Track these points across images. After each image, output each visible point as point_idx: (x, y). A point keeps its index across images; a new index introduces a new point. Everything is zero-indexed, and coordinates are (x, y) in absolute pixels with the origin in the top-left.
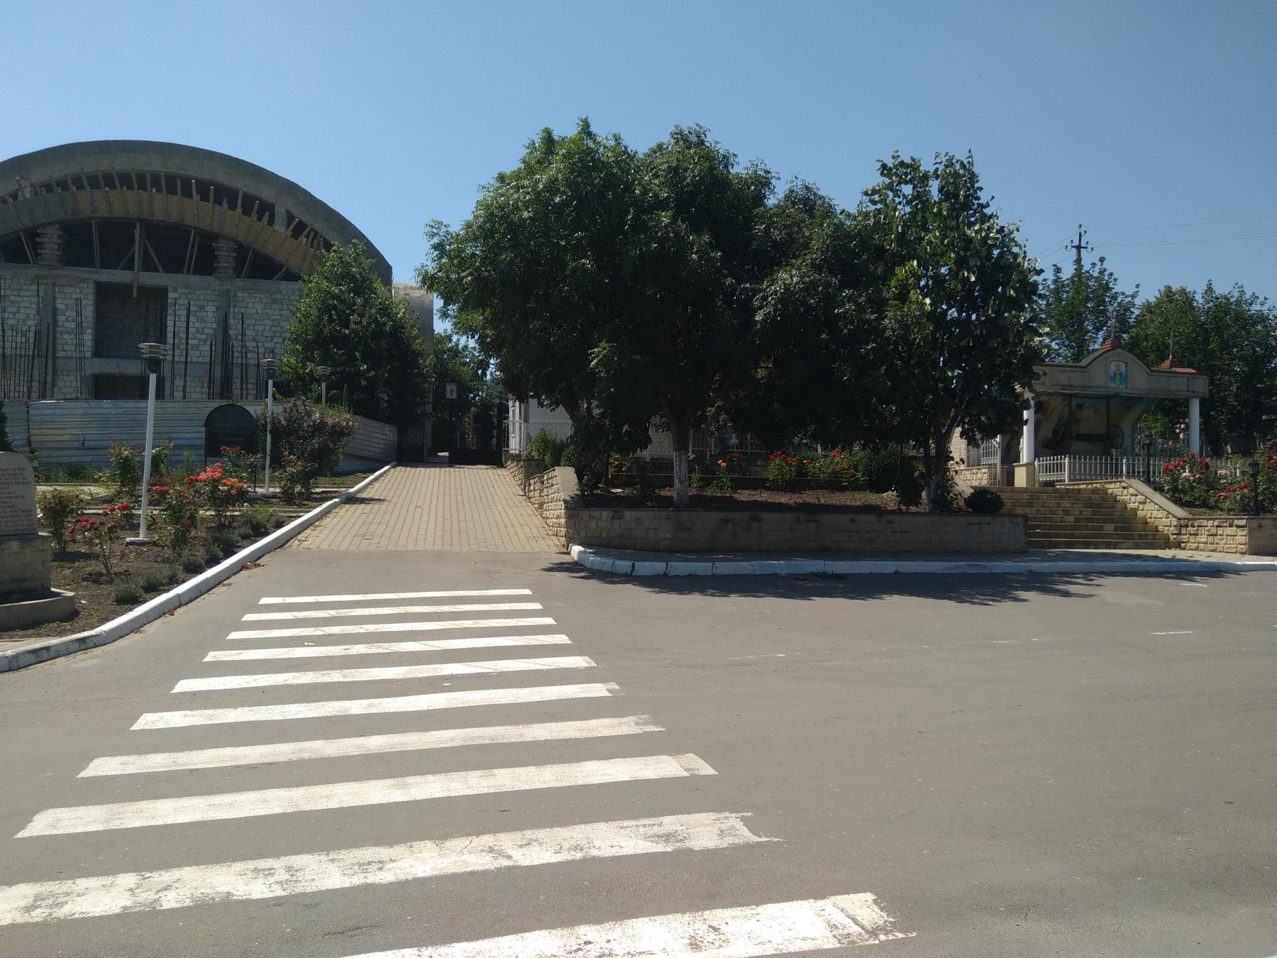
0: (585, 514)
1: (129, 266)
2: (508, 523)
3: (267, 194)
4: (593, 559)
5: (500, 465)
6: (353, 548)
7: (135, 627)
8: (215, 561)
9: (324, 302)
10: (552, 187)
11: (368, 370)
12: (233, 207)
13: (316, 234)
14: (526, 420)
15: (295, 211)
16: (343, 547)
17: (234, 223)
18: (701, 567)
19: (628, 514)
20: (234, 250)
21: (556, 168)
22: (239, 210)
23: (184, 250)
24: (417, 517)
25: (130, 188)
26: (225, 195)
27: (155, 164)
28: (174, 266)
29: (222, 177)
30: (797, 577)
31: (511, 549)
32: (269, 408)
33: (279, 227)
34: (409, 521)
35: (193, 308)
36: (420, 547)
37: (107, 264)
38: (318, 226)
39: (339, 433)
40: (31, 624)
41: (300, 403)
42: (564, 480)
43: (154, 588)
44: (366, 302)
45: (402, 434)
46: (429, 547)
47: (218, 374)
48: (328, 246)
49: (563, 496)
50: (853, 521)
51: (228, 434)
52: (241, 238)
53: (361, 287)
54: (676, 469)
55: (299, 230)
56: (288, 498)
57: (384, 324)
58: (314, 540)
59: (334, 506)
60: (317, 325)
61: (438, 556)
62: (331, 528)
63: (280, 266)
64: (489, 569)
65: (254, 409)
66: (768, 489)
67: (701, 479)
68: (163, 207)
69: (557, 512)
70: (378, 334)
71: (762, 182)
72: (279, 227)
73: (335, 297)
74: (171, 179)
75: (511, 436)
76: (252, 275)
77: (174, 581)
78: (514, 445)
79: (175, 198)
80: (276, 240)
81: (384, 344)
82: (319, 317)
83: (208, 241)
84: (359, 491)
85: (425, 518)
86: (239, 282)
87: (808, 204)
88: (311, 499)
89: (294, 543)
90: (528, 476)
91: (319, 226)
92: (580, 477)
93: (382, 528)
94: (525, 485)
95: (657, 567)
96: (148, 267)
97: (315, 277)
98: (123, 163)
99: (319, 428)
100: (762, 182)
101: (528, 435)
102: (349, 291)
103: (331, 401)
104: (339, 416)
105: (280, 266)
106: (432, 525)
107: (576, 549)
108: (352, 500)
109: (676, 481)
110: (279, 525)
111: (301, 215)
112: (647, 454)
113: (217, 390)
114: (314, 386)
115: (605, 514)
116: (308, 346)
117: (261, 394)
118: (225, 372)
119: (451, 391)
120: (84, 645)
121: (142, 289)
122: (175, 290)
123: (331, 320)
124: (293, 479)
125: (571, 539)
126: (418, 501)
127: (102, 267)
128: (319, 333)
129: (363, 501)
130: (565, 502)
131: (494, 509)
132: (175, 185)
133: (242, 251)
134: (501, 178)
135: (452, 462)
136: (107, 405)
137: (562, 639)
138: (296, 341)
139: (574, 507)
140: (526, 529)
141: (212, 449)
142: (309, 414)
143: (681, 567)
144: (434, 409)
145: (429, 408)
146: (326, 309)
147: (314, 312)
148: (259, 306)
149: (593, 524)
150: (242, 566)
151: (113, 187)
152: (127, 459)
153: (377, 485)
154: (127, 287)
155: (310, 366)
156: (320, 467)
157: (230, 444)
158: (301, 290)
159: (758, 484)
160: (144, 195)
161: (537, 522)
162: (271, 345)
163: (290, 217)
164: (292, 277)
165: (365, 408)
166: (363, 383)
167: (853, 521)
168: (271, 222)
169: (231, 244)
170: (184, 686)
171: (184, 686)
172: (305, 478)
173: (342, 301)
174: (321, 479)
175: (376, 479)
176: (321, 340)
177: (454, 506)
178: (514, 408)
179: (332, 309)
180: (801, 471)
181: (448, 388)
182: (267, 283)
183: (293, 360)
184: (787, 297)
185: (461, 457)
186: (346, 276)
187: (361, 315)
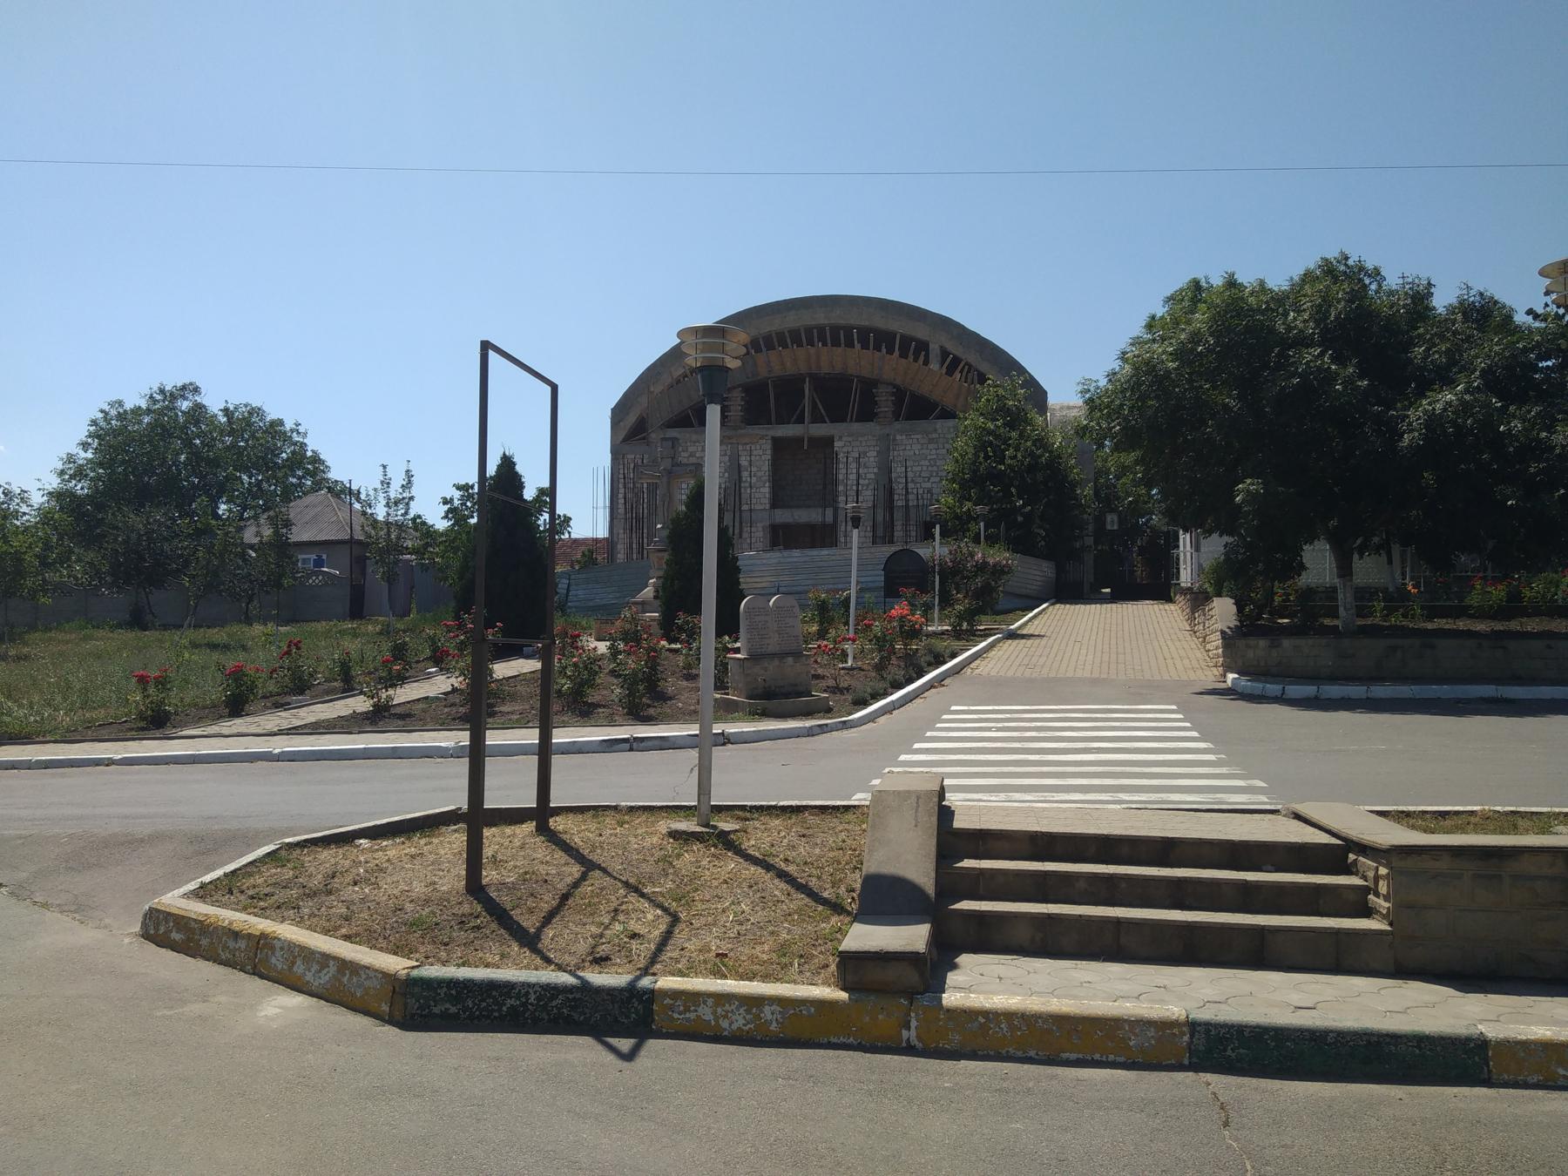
0: (1241, 643)
1: (801, 420)
2: (1167, 655)
3: (920, 332)
4: (1245, 683)
5: (1170, 600)
6: (1019, 674)
7: (871, 718)
8: (911, 681)
9: (979, 438)
10: (1195, 338)
11: (1024, 506)
12: (890, 351)
13: (970, 366)
14: (1197, 549)
15: (949, 346)
16: (1010, 674)
17: (891, 367)
18: (1356, 691)
19: (1287, 643)
20: (893, 394)
21: (1200, 319)
22: (897, 353)
23: (845, 399)
24: (1077, 649)
25: (800, 345)
26: (883, 340)
27: (820, 318)
28: (838, 417)
29: (880, 322)
30: (1459, 701)
31: (1166, 677)
32: (937, 550)
33: (934, 366)
34: (1067, 655)
35: (857, 452)
36: (1079, 674)
37: (781, 421)
38: (971, 362)
39: (1000, 571)
40: (808, 713)
41: (965, 545)
42: (1223, 611)
43: (876, 697)
44: (1021, 436)
45: (1060, 570)
46: (1087, 674)
47: (880, 518)
48: (982, 379)
49: (1219, 626)
50: (1549, 647)
51: (904, 576)
52: (898, 381)
53: (1016, 419)
54: (1340, 596)
55: (953, 364)
56: (957, 634)
57: (1040, 456)
58: (983, 668)
59: (998, 641)
60: (974, 463)
61: (1095, 682)
62: (997, 658)
63: (934, 405)
64: (1141, 691)
65: (924, 551)
66: (1471, 617)
67: (1385, 608)
68: (831, 360)
69: (1216, 641)
70: (1033, 468)
71: (1420, 298)
72: (934, 366)
73: (990, 433)
74: (835, 329)
75: (1182, 567)
76: (911, 417)
77: (885, 694)
78: (1186, 577)
79: (840, 350)
80: (931, 379)
81: (1040, 477)
82: (976, 455)
83: (869, 386)
84: (1020, 627)
85: (1084, 652)
86: (897, 425)
87: (1483, 315)
88: (973, 636)
89: (968, 671)
90: (1194, 609)
91: (971, 357)
92: (1240, 610)
93: (1042, 660)
94: (1191, 619)
95: (1309, 690)
96: (817, 419)
97: (972, 414)
98: (792, 321)
99: (982, 567)
100: (1420, 298)
101: (1200, 566)
102: (1005, 425)
103: (992, 540)
104: (999, 556)
105: (935, 405)
106: (1090, 657)
107: (1231, 676)
108: (1013, 636)
109: (1341, 609)
110: (954, 656)
111: (955, 349)
112: (1305, 580)
113: (880, 533)
114: (972, 526)
115: (1263, 643)
116: (965, 485)
117: (928, 536)
118: (887, 517)
119: (1112, 522)
120: (845, 725)
121: (811, 439)
122: (840, 438)
123: (987, 457)
124: (961, 617)
125: (1228, 668)
126: (1075, 632)
127: (778, 423)
128: (975, 472)
129: (1023, 637)
130: (1223, 632)
131: (1156, 643)
132: (838, 336)
133: (899, 393)
134: (1150, 326)
135: (1115, 598)
136: (796, 554)
137: (1195, 734)
138: (953, 481)
139: (1228, 639)
140: (1186, 662)
141: (891, 590)
142: (972, 555)
143: (1334, 691)
144: (1096, 543)
145: (1089, 541)
146: (982, 446)
147: (971, 450)
148: (916, 447)
149: (1250, 654)
150: (930, 686)
151: (785, 346)
152: (824, 602)
153: (1036, 622)
154: (799, 440)
155: (968, 505)
156: (985, 604)
157: (906, 586)
158: (956, 428)
159: (1461, 612)
160: (812, 350)
161: (1199, 655)
162: (928, 485)
163: (945, 353)
164: (948, 415)
165: (1022, 544)
166: (1020, 519)
167: (1549, 647)
168: (926, 362)
169: (890, 389)
170: (916, 746)
171: (916, 746)
172: (971, 615)
173: (997, 437)
174: (983, 618)
175: (1035, 617)
176: (975, 480)
177: (1113, 641)
178: (1185, 539)
179: (988, 445)
180: (1515, 596)
181: (1109, 518)
182: (923, 424)
183: (950, 500)
184: (1432, 421)
185: (1127, 592)
186: (1003, 410)
187: (1017, 449)
